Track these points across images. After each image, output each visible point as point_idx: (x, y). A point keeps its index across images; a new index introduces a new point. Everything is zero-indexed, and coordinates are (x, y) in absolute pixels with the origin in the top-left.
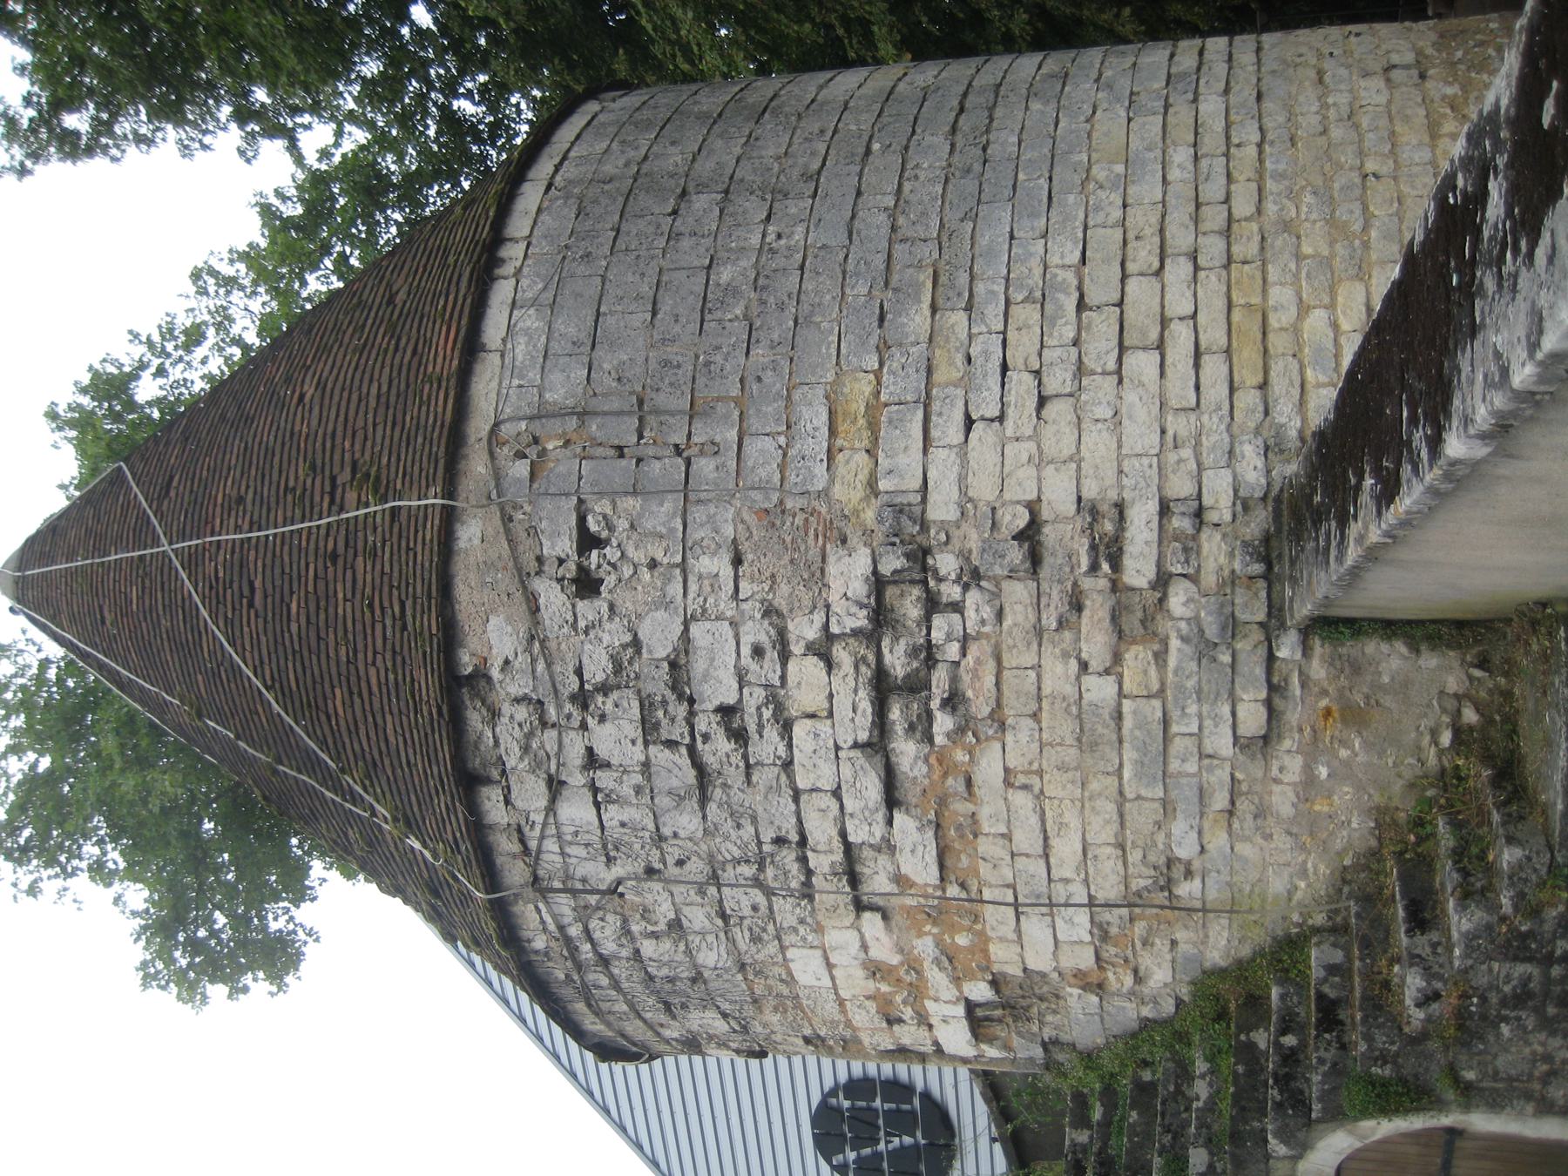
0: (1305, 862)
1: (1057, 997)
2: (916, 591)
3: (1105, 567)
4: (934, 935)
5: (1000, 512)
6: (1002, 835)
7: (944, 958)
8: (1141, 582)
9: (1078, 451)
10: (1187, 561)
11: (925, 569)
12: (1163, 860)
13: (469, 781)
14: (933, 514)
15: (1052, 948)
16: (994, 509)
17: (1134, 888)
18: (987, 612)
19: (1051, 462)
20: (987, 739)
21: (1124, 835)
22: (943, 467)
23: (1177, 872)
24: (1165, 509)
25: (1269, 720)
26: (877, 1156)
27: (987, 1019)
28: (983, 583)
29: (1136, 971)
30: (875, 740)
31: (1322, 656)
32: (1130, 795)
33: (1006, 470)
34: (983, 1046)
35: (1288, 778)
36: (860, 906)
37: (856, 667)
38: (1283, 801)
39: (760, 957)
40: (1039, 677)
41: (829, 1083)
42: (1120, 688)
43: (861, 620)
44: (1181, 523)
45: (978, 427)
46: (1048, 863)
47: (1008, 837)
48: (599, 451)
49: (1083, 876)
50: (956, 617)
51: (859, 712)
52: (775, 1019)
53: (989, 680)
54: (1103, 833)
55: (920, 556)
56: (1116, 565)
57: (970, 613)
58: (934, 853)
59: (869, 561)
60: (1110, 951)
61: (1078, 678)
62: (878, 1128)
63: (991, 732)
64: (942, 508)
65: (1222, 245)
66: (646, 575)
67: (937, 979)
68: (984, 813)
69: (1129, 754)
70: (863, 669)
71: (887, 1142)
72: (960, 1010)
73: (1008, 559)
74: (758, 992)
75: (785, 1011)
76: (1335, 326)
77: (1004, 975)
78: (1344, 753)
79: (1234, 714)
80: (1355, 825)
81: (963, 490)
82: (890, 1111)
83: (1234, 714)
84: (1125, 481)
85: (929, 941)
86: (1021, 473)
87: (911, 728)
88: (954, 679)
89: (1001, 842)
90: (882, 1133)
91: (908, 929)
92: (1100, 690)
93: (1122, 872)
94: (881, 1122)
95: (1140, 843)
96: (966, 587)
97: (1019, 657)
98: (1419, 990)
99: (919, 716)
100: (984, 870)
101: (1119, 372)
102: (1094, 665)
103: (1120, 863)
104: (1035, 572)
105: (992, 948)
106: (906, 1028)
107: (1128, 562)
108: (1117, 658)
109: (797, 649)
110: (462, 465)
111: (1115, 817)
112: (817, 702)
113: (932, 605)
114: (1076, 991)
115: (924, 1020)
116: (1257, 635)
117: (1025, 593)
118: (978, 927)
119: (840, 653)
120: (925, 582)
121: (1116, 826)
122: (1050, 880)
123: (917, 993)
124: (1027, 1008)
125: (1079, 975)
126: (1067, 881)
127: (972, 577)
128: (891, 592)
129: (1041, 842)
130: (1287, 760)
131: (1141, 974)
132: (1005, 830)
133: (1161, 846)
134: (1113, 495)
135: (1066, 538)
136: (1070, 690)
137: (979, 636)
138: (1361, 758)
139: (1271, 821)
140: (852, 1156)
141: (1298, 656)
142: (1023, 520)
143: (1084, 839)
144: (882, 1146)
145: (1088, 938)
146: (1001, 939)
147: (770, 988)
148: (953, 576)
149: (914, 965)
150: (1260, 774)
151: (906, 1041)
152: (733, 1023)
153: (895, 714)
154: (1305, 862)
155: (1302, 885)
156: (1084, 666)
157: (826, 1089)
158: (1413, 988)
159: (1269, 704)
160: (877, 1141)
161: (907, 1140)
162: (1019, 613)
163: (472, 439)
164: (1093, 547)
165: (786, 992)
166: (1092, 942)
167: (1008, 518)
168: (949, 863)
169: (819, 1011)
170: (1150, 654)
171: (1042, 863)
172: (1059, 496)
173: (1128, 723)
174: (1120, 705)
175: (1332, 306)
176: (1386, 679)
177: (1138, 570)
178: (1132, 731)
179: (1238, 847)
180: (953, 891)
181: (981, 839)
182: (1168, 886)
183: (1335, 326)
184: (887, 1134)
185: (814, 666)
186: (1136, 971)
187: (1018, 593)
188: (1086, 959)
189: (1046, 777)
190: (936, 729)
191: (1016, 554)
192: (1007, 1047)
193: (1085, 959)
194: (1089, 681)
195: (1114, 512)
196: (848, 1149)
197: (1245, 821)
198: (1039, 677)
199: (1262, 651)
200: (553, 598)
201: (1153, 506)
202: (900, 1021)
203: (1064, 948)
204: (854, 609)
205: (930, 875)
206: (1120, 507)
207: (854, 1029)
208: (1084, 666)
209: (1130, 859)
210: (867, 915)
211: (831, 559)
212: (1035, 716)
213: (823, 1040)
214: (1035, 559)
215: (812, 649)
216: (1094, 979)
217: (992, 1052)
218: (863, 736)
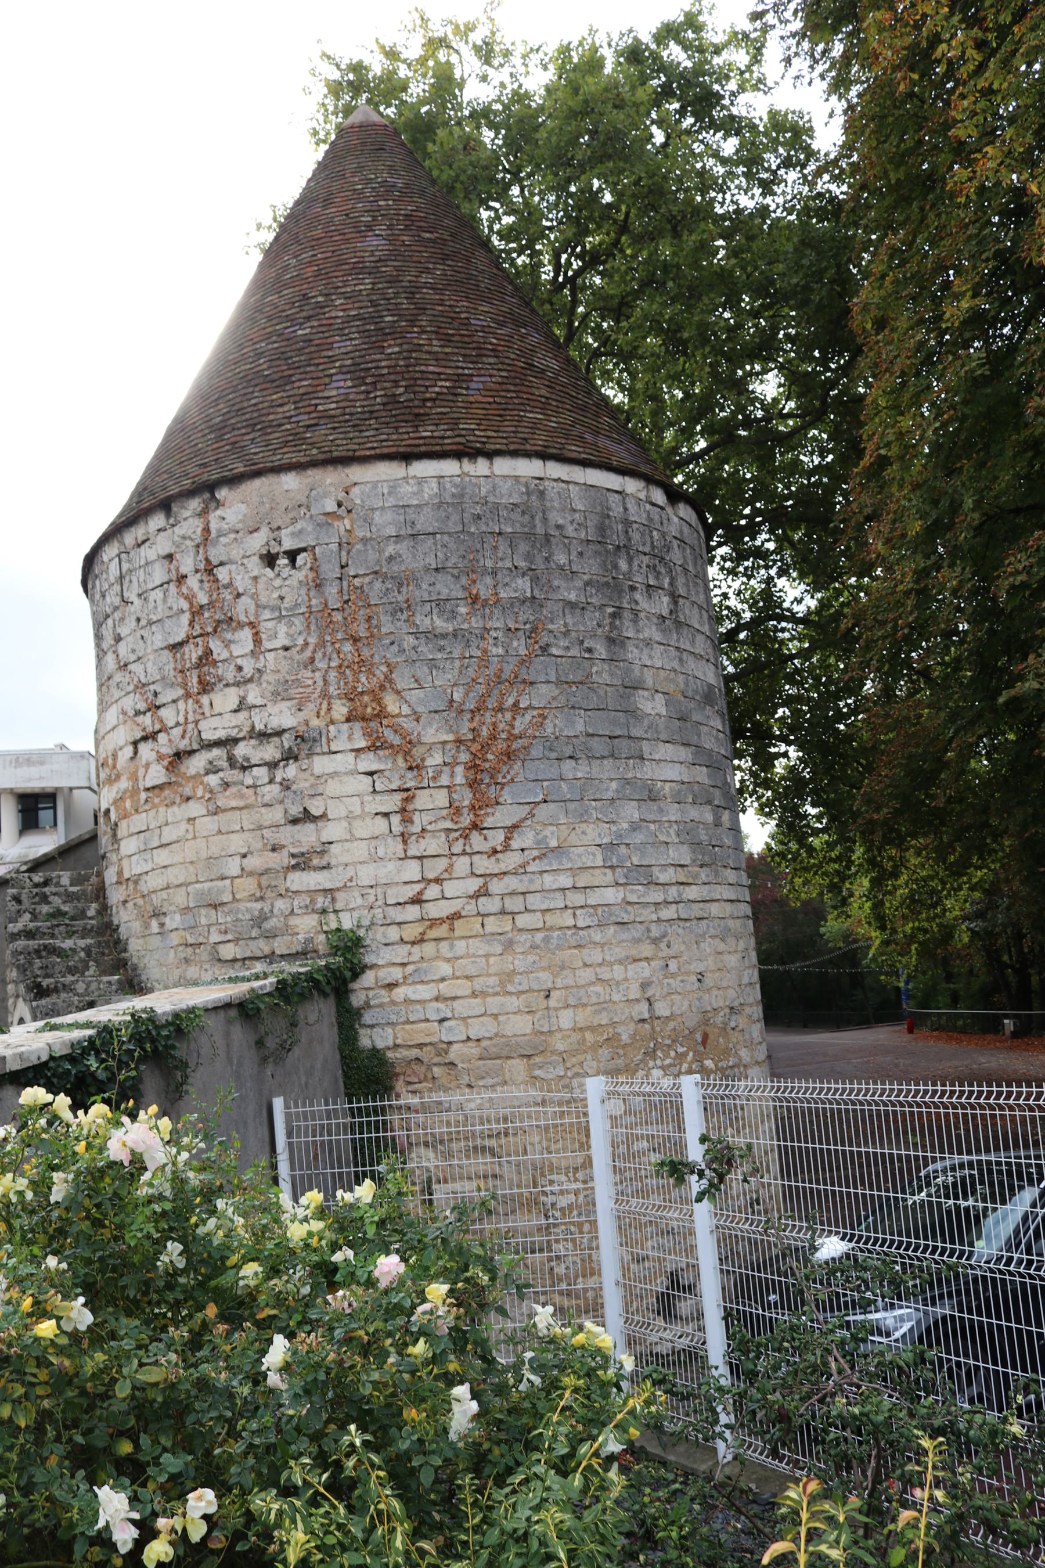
13: (166, 506)
18: (267, 799)
22: (344, 762)
32: (190, 889)
36: (135, 744)
43: (259, 727)
44: (321, 902)
45: (368, 780)
48: (344, 553)
56: (295, 867)
57: (268, 788)
64: (321, 764)
65: (494, 910)
66: (275, 595)
68: (175, 808)
76: (443, 980)
81: (334, 775)
86: (342, 808)
88: (235, 784)
97: (247, 819)
100: (152, 813)
101: (406, 857)
102: (245, 861)
108: (251, 874)
110: (330, 468)
113: (273, 765)
116: (267, 950)
119: (242, 715)
127: (286, 786)
134: (333, 862)
135: (306, 836)
136: (232, 850)
142: (316, 812)
153: (216, 752)
156: (244, 856)
163: (347, 470)
173: (220, 883)
175: (455, 977)
177: (299, 880)
180: (143, 796)
183: (443, 980)
185: (234, 703)
187: (276, 815)
191: (295, 810)
194: (237, 859)
195: (324, 863)
199: (259, 954)
200: (258, 542)
201: (328, 885)
206: (327, 867)
208: (244, 856)
211: (288, 704)
212: (220, 832)
214: (295, 821)
215: (242, 701)
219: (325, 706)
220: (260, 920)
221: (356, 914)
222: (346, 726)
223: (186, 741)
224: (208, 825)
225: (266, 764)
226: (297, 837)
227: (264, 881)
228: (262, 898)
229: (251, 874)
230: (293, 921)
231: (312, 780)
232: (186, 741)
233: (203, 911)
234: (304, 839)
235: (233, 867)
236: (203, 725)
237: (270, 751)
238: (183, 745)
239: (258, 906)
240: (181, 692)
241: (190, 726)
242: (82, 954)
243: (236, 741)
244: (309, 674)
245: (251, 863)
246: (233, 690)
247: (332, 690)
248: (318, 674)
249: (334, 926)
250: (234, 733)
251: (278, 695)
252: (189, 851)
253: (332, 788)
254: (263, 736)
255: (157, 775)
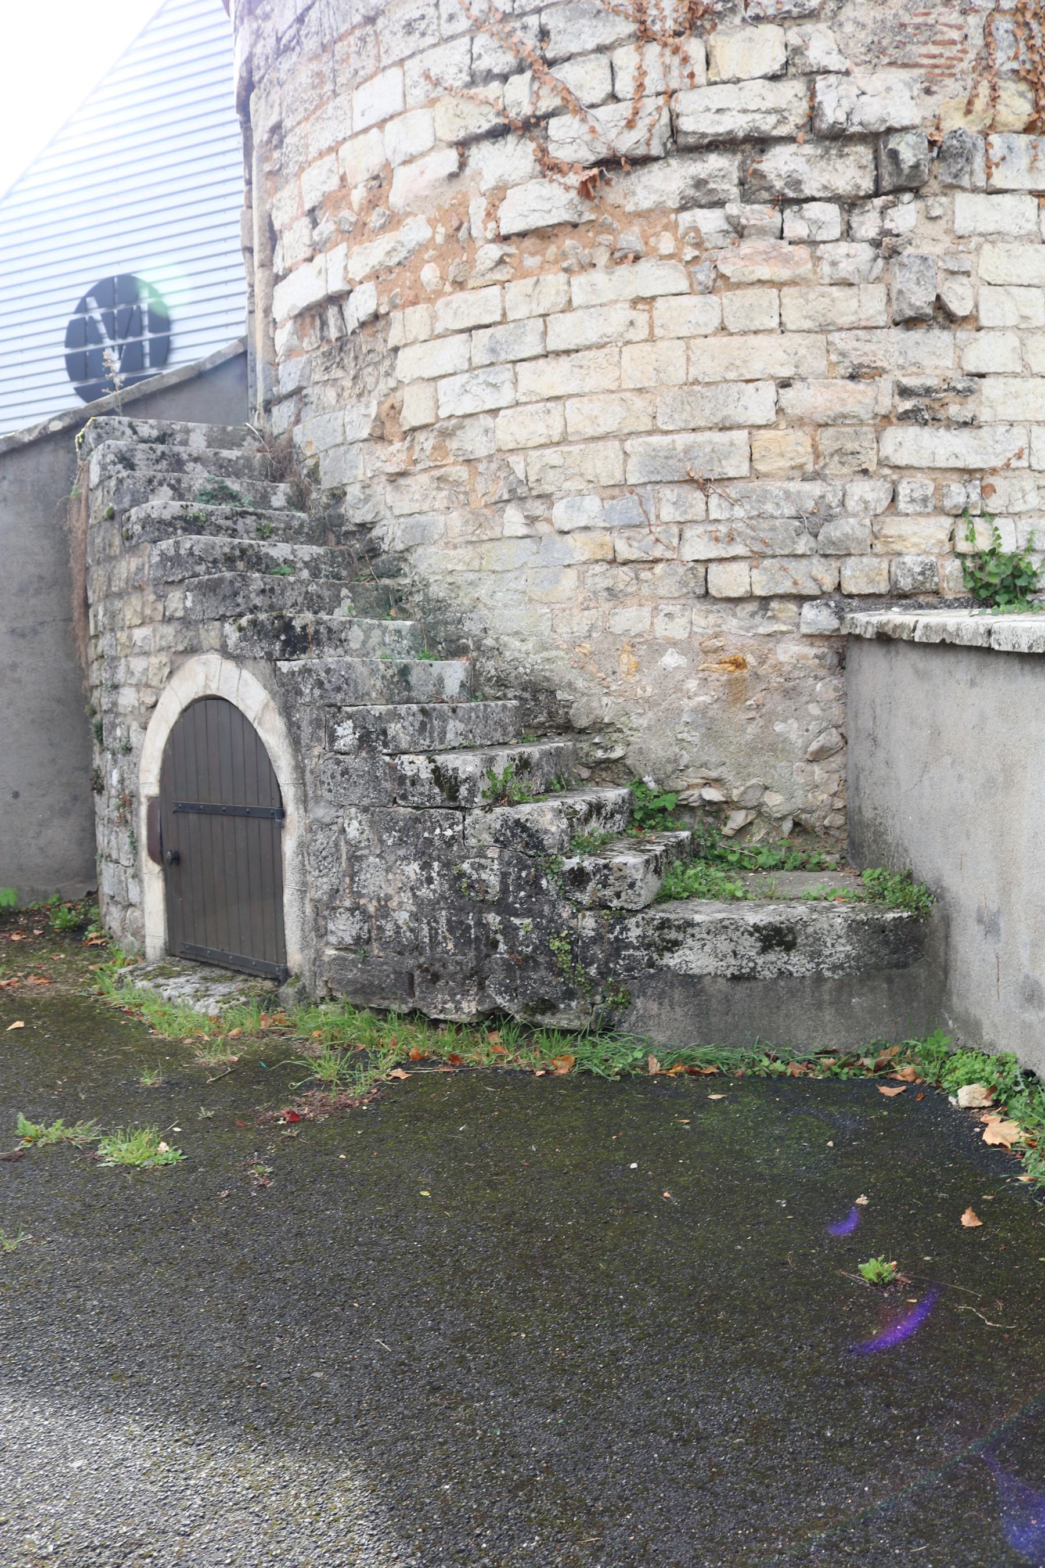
0: (558, 648)
1: (360, 395)
2: (867, 185)
3: (908, 405)
4: (433, 238)
5: (964, 280)
6: (570, 301)
7: (403, 254)
8: (888, 448)
9: (1033, 375)
10: (912, 501)
11: (898, 190)
12: (548, 489)
14: (961, 199)
15: (426, 376)
16: (967, 274)
17: (512, 459)
18: (846, 269)
19: (1023, 344)
20: (690, 276)
21: (577, 442)
23: (537, 508)
24: (968, 473)
25: (729, 600)
26: (99, 339)
27: (324, 324)
28: (880, 262)
29: (403, 474)
30: (681, 140)
31: (805, 657)
32: (628, 445)
33: (1014, 290)
34: (289, 325)
35: (660, 622)
37: (776, 111)
38: (629, 619)
39: (386, 37)
40: (771, 331)
41: (161, 288)
42: (759, 427)
43: (832, 114)
44: (957, 494)
46: (535, 358)
47: (569, 307)
49: (523, 399)
50: (836, 232)
51: (717, 117)
52: (304, 77)
53: (764, 272)
54: (579, 417)
55: (911, 185)
56: (905, 417)
57: (844, 247)
58: (541, 223)
59: (906, 122)
60: (427, 441)
61: (773, 377)
62: (125, 337)
63: (701, 277)
64: (969, 211)
67: (376, 252)
68: (598, 276)
69: (682, 440)
70: (772, 119)
71: (113, 347)
72: (336, 285)
73: (915, 288)
74: (338, 47)
75: (314, 87)
77: (389, 324)
78: (692, 685)
79: (734, 559)
80: (605, 700)
81: (993, 237)
82: (142, 347)
83: (734, 559)
84: (1001, 429)
85: (426, 233)
87: (700, 183)
88: (762, 231)
89: (562, 301)
90: (120, 341)
91: (439, 208)
92: (758, 404)
93: (530, 444)
94: (130, 340)
95: (569, 461)
96: (876, 244)
97: (796, 309)
98: (455, 769)
99: (712, 191)
100: (517, 289)
102: (787, 394)
103: (543, 441)
104: (896, 324)
105: (421, 308)
106: (306, 232)
107: (911, 433)
108: (798, 422)
109: (793, 36)
111: (601, 431)
112: (727, 64)
113: (850, 204)
114: (373, 411)
115: (316, 249)
117: (871, 312)
118: (448, 288)
119: (791, 92)
120: (877, 194)
121: (590, 432)
122: (514, 362)
123: (357, 232)
124: (341, 365)
125: (395, 410)
126: (515, 382)
127: (888, 248)
128: (863, 153)
129: (563, 347)
130: (681, 621)
131: (402, 481)
132: (575, 304)
133: (567, 485)
137: (817, 260)
138: (687, 704)
139: (606, 606)
140: (97, 315)
141: (804, 630)
142: (959, 308)
143: (570, 396)
144: (108, 342)
145: (443, 413)
146: (434, 318)
147: (345, 60)
148: (888, 225)
149: (393, 221)
150: (662, 592)
151: (287, 239)
152: (292, 32)
153: (715, 162)
154: (558, 648)
155: (529, 646)
156: (785, 384)
157: (155, 286)
158: (458, 763)
159: (750, 598)
160: (112, 337)
161: (117, 366)
162: (846, 306)
164: (928, 391)
165: (341, 80)
166: (438, 419)
167: (960, 290)
168: (528, 243)
169: (318, 126)
170: (803, 460)
171: (539, 350)
172: (985, 352)
173: (718, 437)
174: (740, 427)
176: (779, 727)
177: (907, 444)
178: (710, 442)
179: (572, 573)
181: (563, 277)
182: (515, 497)
184: (120, 347)
185: (773, 59)
186: (403, 474)
187: (872, 304)
188: (414, 414)
189: (647, 347)
190: (699, 213)
191: (921, 299)
192: (290, 352)
193: (414, 414)
194: (769, 390)
195: (967, 415)
196: (103, 310)
197: (600, 578)
198: (771, 331)
202: (315, 224)
203: (428, 389)
204: (846, 105)
205: (511, 222)
207: (297, 175)
208: (785, 384)
209: (547, 452)
210: (453, 155)
211: (905, 74)
213: (280, 144)
214: (910, 323)
216: (389, 429)
217: (283, 337)
218: (686, 124)
219: (984, 90)
220: (813, 521)
221: (1025, 525)
222: (1024, 139)
223: (639, 133)
224: (700, 312)
225: (835, 199)
226: (913, 355)
227: (827, 440)
228: (817, 476)
229: (798, 422)
230: (892, 527)
231: (947, 241)
232: (639, 133)
233: (668, 493)
234: (928, 362)
235: (758, 404)
236: (685, 102)
237: (850, 172)
238: (627, 143)
239: (815, 489)
240: (632, 27)
241: (650, 104)
242: (305, 574)
243: (761, 143)
244: (955, 17)
245: (799, 399)
246: (770, 32)
247: (1002, 59)
248: (972, 20)
249: (983, 544)
250: (767, 124)
251: (879, 54)
252: (636, 365)
253: (991, 262)
254: (837, 138)
255: (547, 202)
